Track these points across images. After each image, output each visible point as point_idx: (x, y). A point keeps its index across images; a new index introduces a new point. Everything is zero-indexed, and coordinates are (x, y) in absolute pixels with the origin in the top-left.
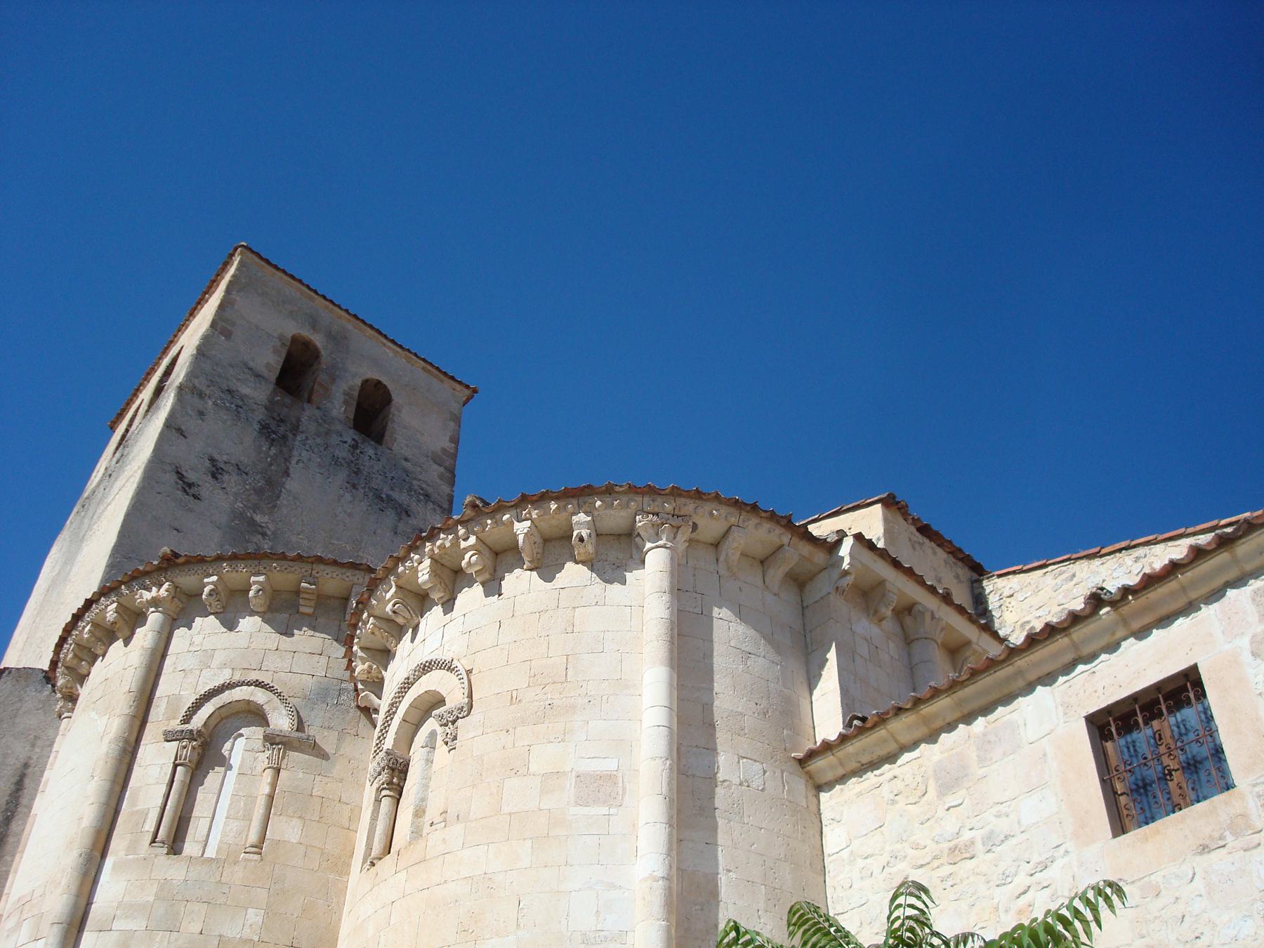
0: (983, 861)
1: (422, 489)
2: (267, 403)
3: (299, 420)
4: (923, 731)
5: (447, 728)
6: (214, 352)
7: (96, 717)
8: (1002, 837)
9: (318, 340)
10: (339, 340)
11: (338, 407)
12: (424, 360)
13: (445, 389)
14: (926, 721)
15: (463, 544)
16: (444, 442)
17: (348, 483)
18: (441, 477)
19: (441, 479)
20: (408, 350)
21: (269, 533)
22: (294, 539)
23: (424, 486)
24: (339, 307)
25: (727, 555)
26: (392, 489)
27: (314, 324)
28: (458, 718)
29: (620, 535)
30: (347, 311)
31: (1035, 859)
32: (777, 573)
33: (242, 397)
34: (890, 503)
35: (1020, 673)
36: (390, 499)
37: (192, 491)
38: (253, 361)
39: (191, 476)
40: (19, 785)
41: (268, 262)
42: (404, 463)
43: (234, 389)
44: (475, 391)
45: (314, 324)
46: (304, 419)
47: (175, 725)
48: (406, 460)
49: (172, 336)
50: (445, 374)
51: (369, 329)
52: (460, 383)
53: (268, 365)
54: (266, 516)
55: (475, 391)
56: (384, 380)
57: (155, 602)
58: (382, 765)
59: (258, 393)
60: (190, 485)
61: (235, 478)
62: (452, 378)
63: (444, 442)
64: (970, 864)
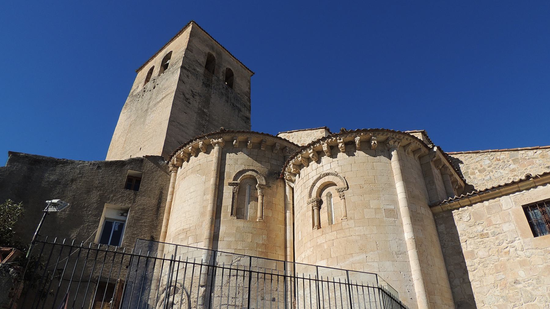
0: (492, 238)
1: (243, 103)
2: (204, 74)
3: (212, 80)
4: (469, 203)
5: (340, 193)
6: (189, 56)
7: (200, 176)
8: (497, 233)
9: (214, 54)
10: (219, 54)
11: (221, 76)
12: (241, 63)
13: (246, 72)
14: (470, 201)
15: (338, 141)
16: (247, 89)
17: (226, 100)
18: (247, 100)
19: (247, 101)
20: (237, 60)
21: (208, 115)
22: (214, 117)
23: (244, 102)
24: (219, 44)
25: (408, 150)
26: (236, 103)
27: (212, 48)
28: (344, 190)
29: (381, 142)
30: (221, 45)
31: (509, 240)
32: (417, 156)
33: (198, 72)
34: (423, 133)
35: (501, 192)
36: (236, 107)
37: (188, 101)
38: (199, 60)
39: (187, 96)
40: (161, 193)
41: (200, 27)
42: (238, 94)
43: (195, 69)
44: (254, 74)
45: (212, 48)
46: (213, 80)
47: (231, 181)
48: (239, 94)
49: (164, 46)
50: (246, 68)
51: (227, 52)
52: (250, 71)
53: (203, 62)
54: (207, 110)
55: (254, 74)
56: (231, 68)
57: (218, 143)
58: (314, 200)
59: (201, 70)
60: (187, 99)
61: (198, 97)
62: (248, 69)
63: (247, 89)
64: (487, 239)
